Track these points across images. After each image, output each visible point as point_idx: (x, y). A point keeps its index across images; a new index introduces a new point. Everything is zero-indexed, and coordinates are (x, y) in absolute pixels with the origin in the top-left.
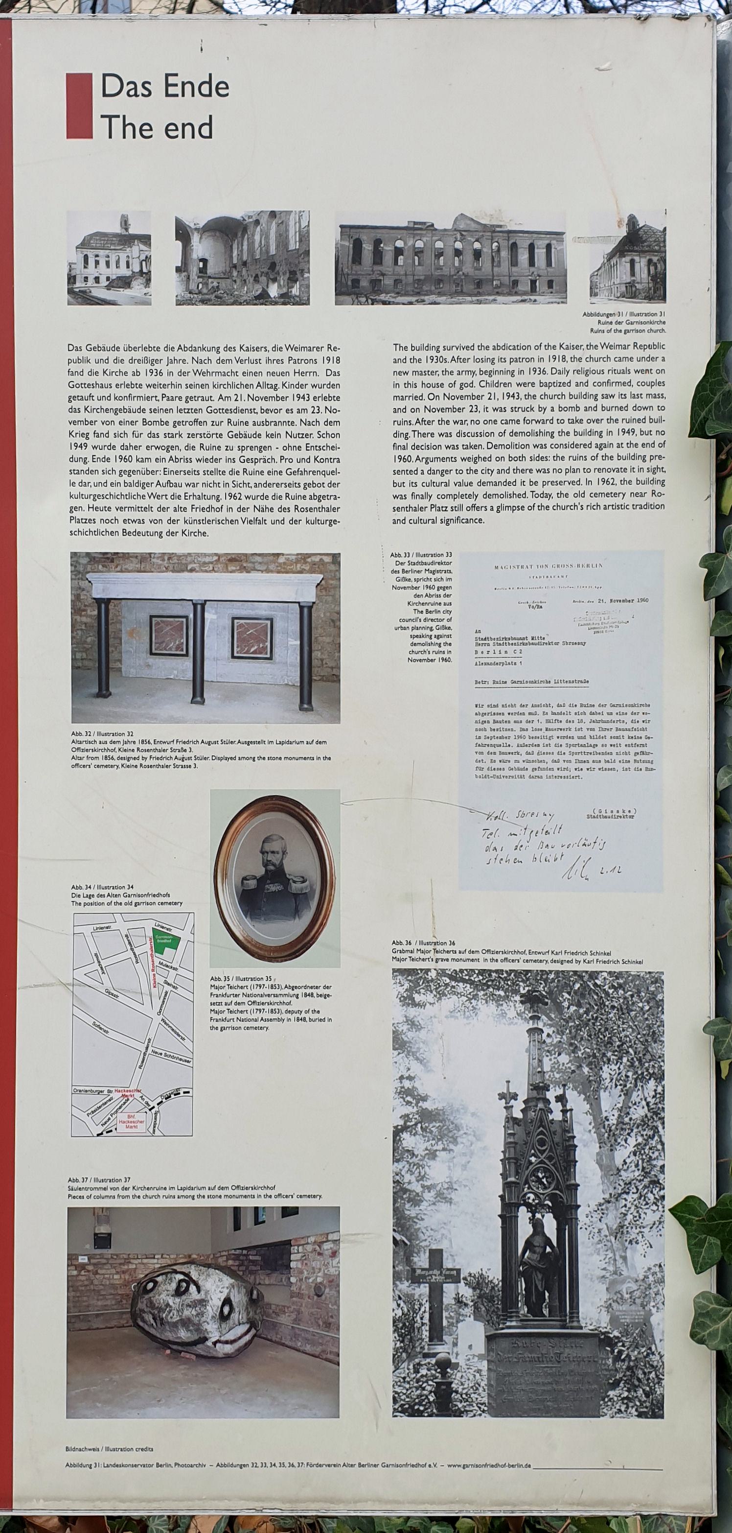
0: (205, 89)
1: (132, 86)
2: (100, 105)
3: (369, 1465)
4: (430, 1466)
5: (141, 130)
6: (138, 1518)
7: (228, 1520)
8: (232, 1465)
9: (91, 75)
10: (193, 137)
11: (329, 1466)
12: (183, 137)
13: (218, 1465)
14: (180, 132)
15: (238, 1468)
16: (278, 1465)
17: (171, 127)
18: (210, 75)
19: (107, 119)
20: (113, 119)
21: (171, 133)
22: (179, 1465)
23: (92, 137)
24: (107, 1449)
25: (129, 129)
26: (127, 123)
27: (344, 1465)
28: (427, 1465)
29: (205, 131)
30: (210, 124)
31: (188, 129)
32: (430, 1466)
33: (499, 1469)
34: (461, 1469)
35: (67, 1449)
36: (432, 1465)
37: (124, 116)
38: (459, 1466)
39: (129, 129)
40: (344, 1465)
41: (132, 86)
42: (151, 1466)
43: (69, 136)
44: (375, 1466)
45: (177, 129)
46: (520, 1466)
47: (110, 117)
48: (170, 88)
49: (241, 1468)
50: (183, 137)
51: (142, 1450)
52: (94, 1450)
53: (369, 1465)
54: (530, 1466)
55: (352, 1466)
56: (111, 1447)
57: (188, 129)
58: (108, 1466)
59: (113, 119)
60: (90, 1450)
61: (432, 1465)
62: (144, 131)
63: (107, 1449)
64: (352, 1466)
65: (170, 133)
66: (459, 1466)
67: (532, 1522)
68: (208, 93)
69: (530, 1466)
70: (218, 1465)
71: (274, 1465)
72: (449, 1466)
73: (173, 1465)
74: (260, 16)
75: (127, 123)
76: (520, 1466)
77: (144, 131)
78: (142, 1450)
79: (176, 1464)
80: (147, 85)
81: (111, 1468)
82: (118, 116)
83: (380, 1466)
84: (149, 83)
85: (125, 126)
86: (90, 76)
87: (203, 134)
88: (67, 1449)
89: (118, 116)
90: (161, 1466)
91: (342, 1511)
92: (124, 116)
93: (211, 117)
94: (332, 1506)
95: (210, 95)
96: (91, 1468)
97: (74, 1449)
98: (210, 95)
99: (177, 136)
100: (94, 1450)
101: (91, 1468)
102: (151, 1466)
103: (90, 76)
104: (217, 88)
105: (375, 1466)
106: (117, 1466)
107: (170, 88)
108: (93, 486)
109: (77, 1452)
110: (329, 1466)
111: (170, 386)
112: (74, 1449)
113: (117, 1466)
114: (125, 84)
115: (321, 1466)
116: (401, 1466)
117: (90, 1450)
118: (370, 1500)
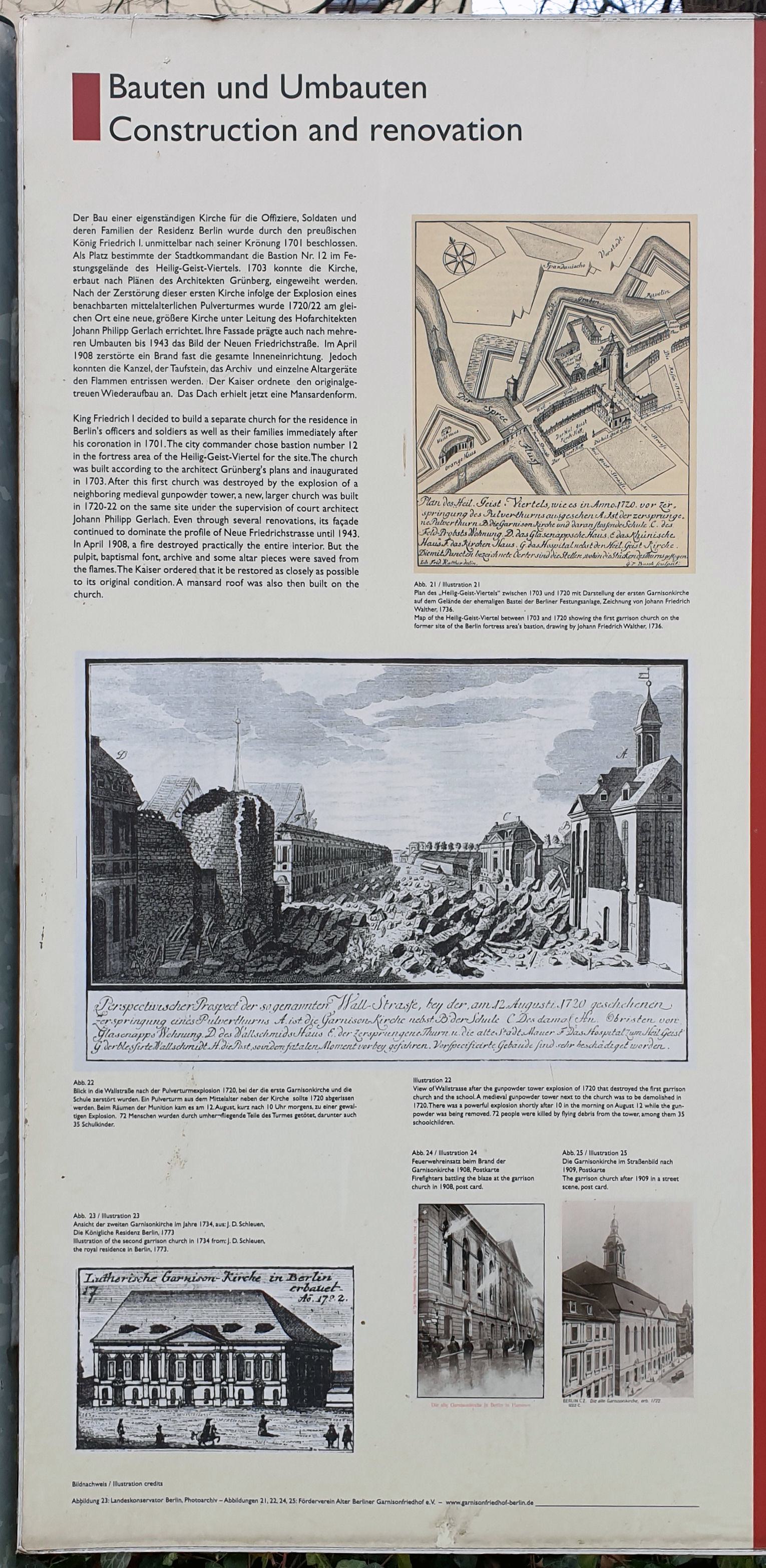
2: (108, 108)
3: (364, 1502)
4: (427, 1503)
6: (711, 1557)
7: (129, 1559)
8: (240, 1501)
9: (98, 75)
10: (337, 139)
12: (403, 139)
13: (226, 1500)
16: (288, 1501)
21: (390, 135)
22: (189, 1499)
23: (99, 139)
24: (116, 1484)
27: (338, 1501)
28: (425, 1502)
30: (355, 126)
31: (408, 131)
32: (427, 1503)
33: (500, 1506)
35: (74, 1484)
36: (430, 1502)
38: (458, 1503)
40: (338, 1501)
41: (356, 87)
42: (161, 1501)
43: (76, 137)
44: (370, 1502)
45: (396, 131)
46: (522, 1503)
48: (115, 89)
50: (403, 139)
51: (151, 1484)
52: (101, 1485)
53: (364, 1502)
54: (532, 1503)
55: (346, 1502)
56: (119, 1482)
57: (408, 131)
58: (115, 1501)
60: (97, 1485)
61: (430, 1502)
63: (116, 1484)
64: (346, 1502)
65: (389, 135)
66: (458, 1503)
67: (96, 1557)
68: (263, 94)
69: (532, 1503)
70: (226, 1500)
71: (285, 1501)
72: (448, 1503)
73: (183, 1500)
74: (528, 16)
76: (522, 1503)
78: (151, 1484)
79: (186, 1499)
81: (118, 1504)
83: (375, 1503)
86: (97, 76)
87: (348, 136)
88: (74, 1484)
91: (174, 1548)
94: (226, 1544)
96: (98, 1503)
97: (81, 1485)
99: (396, 138)
100: (101, 1485)
101: (98, 1503)
102: (161, 1501)
103: (97, 76)
105: (370, 1502)
106: (125, 1501)
107: (115, 89)
108: (237, 498)
110: (322, 1502)
111: (228, 395)
112: (81, 1485)
113: (125, 1501)
114: (348, 86)
115: (313, 1502)
117: (97, 1485)
118: (270, 1539)
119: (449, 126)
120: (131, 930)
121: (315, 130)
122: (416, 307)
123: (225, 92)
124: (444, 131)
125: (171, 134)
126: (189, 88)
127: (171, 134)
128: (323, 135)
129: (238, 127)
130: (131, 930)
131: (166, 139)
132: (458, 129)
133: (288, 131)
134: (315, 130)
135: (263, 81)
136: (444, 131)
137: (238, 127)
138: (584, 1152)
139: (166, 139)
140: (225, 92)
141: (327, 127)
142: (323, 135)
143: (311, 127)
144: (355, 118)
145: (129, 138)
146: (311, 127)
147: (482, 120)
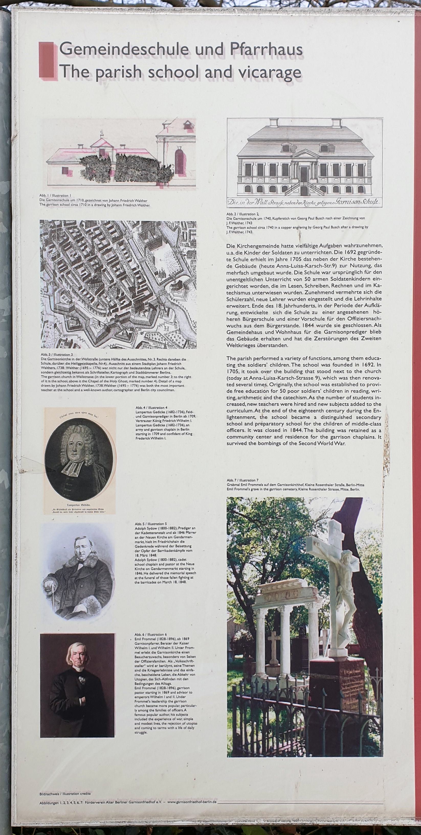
0: (126, 51)
1: (282, 49)
2: (61, 59)
3: (122, 802)
5: (82, 73)
11: (98, 803)
14: (82, 52)
15: (52, 805)
17: (85, 71)
18: (129, 43)
19: (63, 67)
20: (66, 67)
24: (64, 794)
25: (75, 72)
26: (136, 69)
29: (228, 73)
32: (157, 802)
33: (197, 804)
34: (175, 804)
37: (73, 65)
38: (175, 802)
39: (75, 72)
41: (282, 49)
47: (65, 66)
49: (54, 804)
51: (84, 794)
52: (56, 794)
59: (66, 67)
62: (84, 73)
63: (64, 794)
66: (175, 802)
69: (216, 802)
75: (136, 69)
77: (84, 73)
78: (84, 794)
80: (300, 49)
82: (69, 65)
84: (301, 48)
85: (73, 70)
89: (69, 65)
90: (118, 803)
92: (73, 65)
93: (231, 66)
95: (129, 54)
98: (129, 54)
100: (56, 794)
104: (133, 50)
109: (46, 796)
116: (140, 802)
119: (245, 70)
120: (261, 745)
121: (208, 72)
122: (149, 153)
123: (200, 51)
124: (243, 73)
125: (125, 74)
126: (83, 49)
127: (125, 74)
128: (113, 75)
129: (258, 70)
130: (261, 745)
131: (123, 77)
132: (279, 72)
133: (195, 74)
134: (208, 72)
135: (127, 46)
136: (243, 73)
137: (258, 70)
138: (145, 524)
139: (123, 77)
140: (200, 51)
141: (215, 71)
142: (113, 75)
143: (206, 70)
144: (231, 66)
145: (258, 77)
146: (206, 70)
147: (249, 67)
